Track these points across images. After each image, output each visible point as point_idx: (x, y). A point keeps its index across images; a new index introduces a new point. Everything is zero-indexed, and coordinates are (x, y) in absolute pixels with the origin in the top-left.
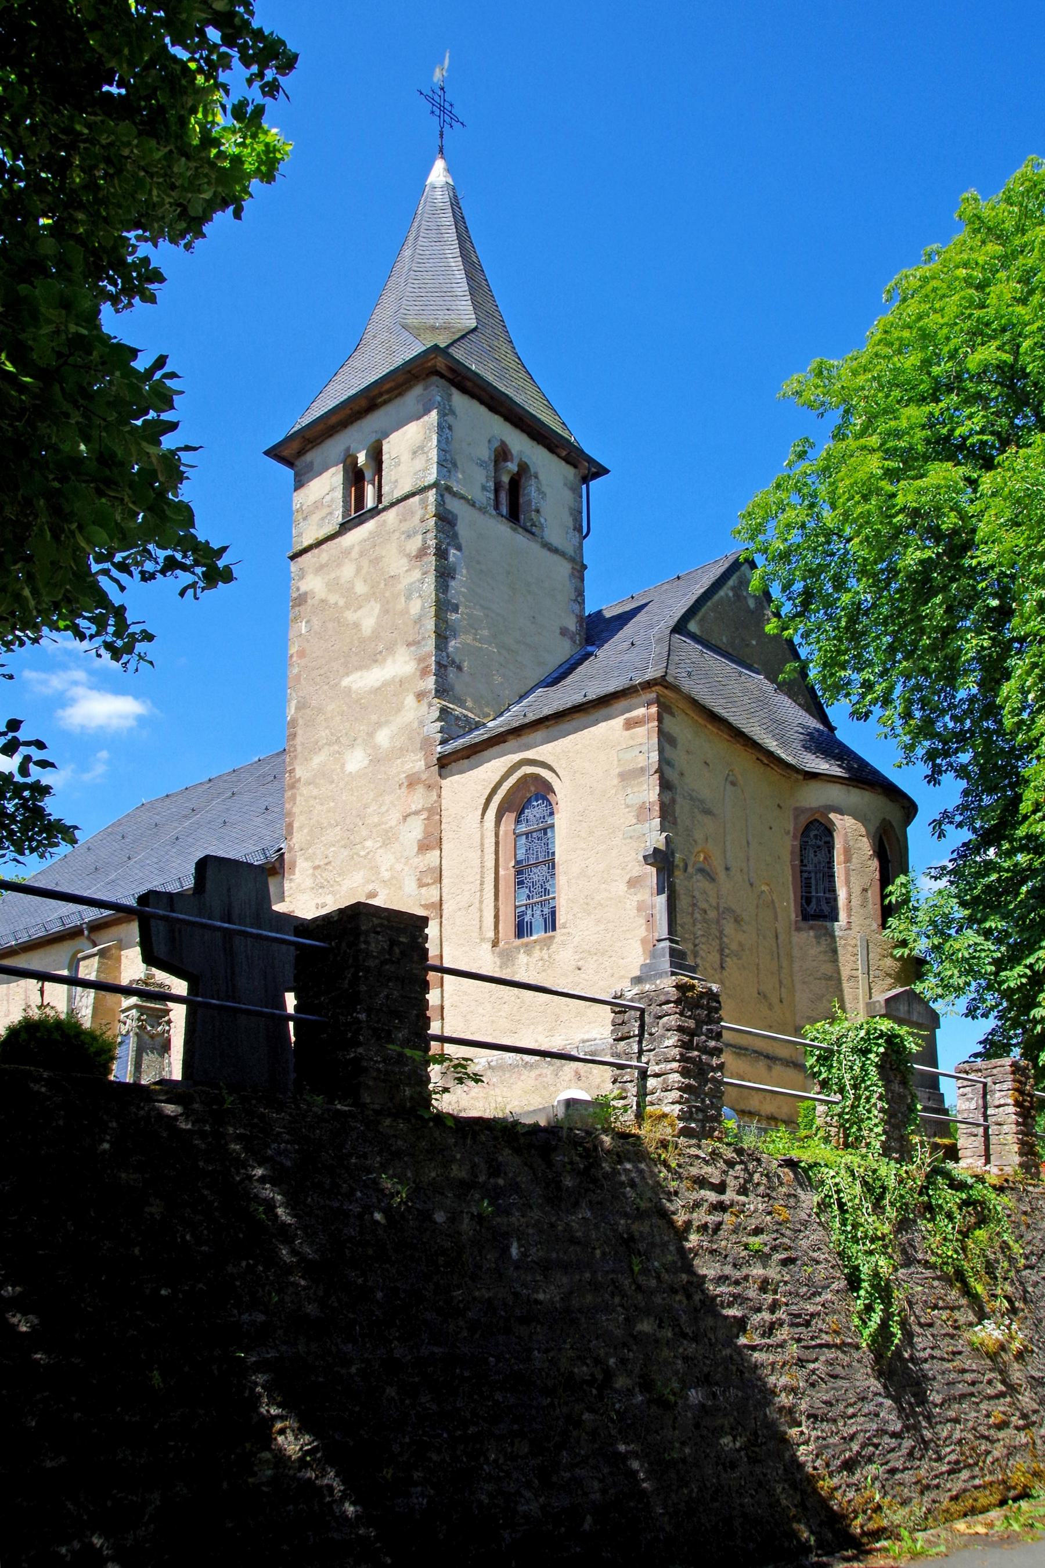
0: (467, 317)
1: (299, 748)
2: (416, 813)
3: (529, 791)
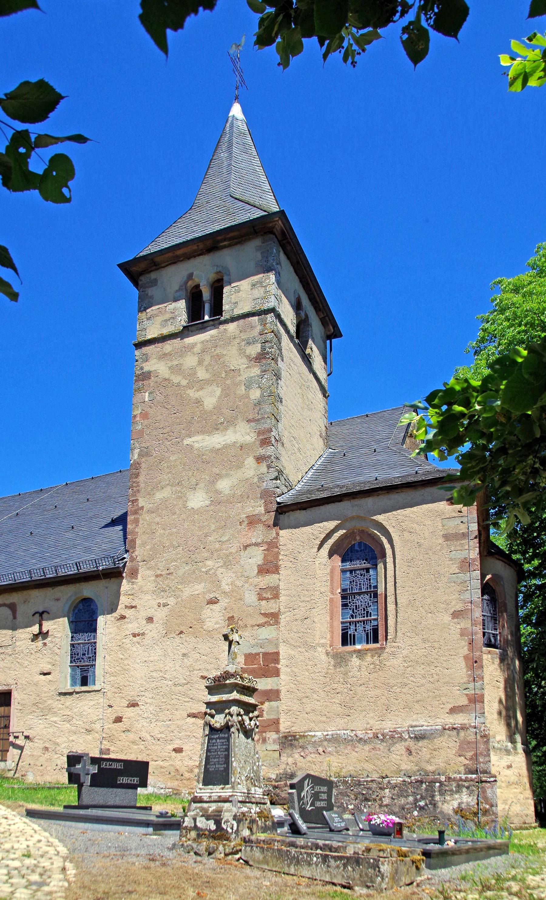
0: (274, 206)
1: (142, 485)
2: (256, 544)
3: (355, 540)
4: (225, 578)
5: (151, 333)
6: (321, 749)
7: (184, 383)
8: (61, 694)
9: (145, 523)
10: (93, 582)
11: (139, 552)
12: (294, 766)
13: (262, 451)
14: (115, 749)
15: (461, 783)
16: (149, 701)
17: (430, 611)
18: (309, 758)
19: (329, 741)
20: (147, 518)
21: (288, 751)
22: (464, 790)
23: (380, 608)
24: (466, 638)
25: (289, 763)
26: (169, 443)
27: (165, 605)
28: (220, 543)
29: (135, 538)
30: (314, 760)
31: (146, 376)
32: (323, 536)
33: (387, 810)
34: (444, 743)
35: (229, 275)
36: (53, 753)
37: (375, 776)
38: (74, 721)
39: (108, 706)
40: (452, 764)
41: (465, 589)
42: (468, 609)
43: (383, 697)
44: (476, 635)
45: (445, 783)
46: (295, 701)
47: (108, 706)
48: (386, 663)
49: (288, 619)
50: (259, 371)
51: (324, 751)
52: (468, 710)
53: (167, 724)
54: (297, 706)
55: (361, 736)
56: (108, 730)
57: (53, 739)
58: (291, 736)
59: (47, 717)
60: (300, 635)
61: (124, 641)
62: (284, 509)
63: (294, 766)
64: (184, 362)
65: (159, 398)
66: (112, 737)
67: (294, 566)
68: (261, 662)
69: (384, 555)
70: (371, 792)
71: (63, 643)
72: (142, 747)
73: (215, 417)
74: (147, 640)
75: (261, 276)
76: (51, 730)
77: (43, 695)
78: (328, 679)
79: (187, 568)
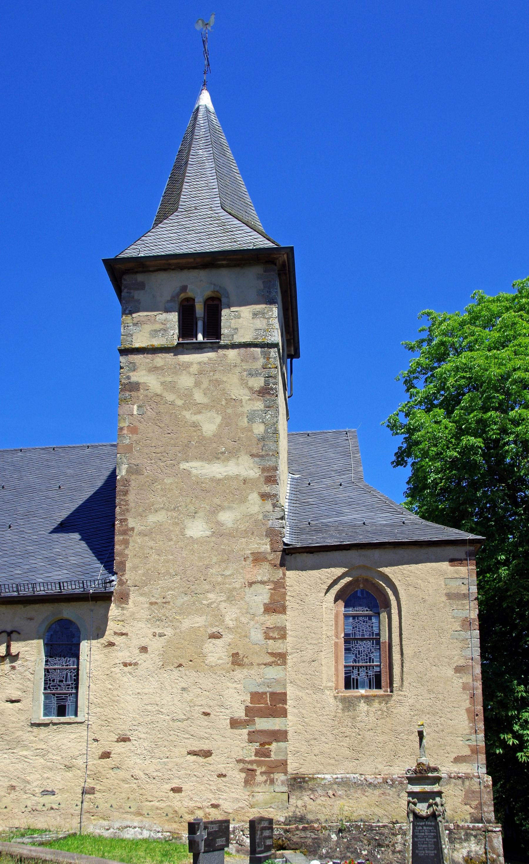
1: (132, 505)
2: (262, 583)
3: (359, 587)
4: (229, 613)
5: (138, 341)
6: (331, 793)
7: (179, 402)
8: (33, 725)
9: (137, 545)
10: (75, 603)
11: (129, 576)
12: (304, 808)
13: (267, 489)
14: (101, 788)
15: (468, 831)
16: (143, 736)
17: (434, 664)
18: (319, 801)
19: (339, 784)
20: (139, 541)
21: (297, 793)
22: (472, 838)
23: (383, 655)
24: (468, 692)
25: (299, 806)
26: (162, 464)
27: (161, 635)
28: (223, 577)
29: (125, 561)
30: (324, 803)
31: (134, 387)
32: (330, 582)
33: (400, 856)
34: (450, 791)
35: (228, 297)
36: (22, 792)
37: (385, 821)
38: (50, 756)
39: (94, 739)
40: (459, 812)
41: (467, 646)
42: (469, 665)
43: (391, 743)
44: (477, 690)
45: (454, 830)
46: (303, 743)
47: (94, 739)
48: (393, 710)
49: (295, 660)
50: (263, 405)
51: (334, 795)
52: (470, 760)
53: (164, 762)
54: (305, 747)
55: (370, 781)
56: (93, 766)
57: (23, 776)
58: (300, 778)
59: (15, 751)
60: (308, 677)
61: (113, 669)
62: (293, 551)
63: (304, 808)
64: (179, 380)
65: (150, 413)
66: (97, 775)
67: (301, 608)
68: (268, 702)
69: (387, 605)
70: (384, 838)
71: (37, 668)
72: (135, 786)
73: (215, 445)
74: (141, 671)
75: (263, 306)
76: (19, 766)
77: (11, 725)
78: (336, 722)
79: (185, 599)
